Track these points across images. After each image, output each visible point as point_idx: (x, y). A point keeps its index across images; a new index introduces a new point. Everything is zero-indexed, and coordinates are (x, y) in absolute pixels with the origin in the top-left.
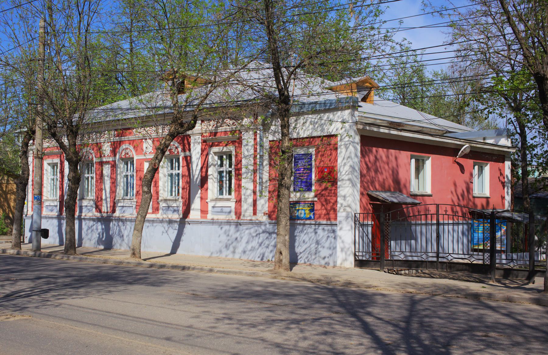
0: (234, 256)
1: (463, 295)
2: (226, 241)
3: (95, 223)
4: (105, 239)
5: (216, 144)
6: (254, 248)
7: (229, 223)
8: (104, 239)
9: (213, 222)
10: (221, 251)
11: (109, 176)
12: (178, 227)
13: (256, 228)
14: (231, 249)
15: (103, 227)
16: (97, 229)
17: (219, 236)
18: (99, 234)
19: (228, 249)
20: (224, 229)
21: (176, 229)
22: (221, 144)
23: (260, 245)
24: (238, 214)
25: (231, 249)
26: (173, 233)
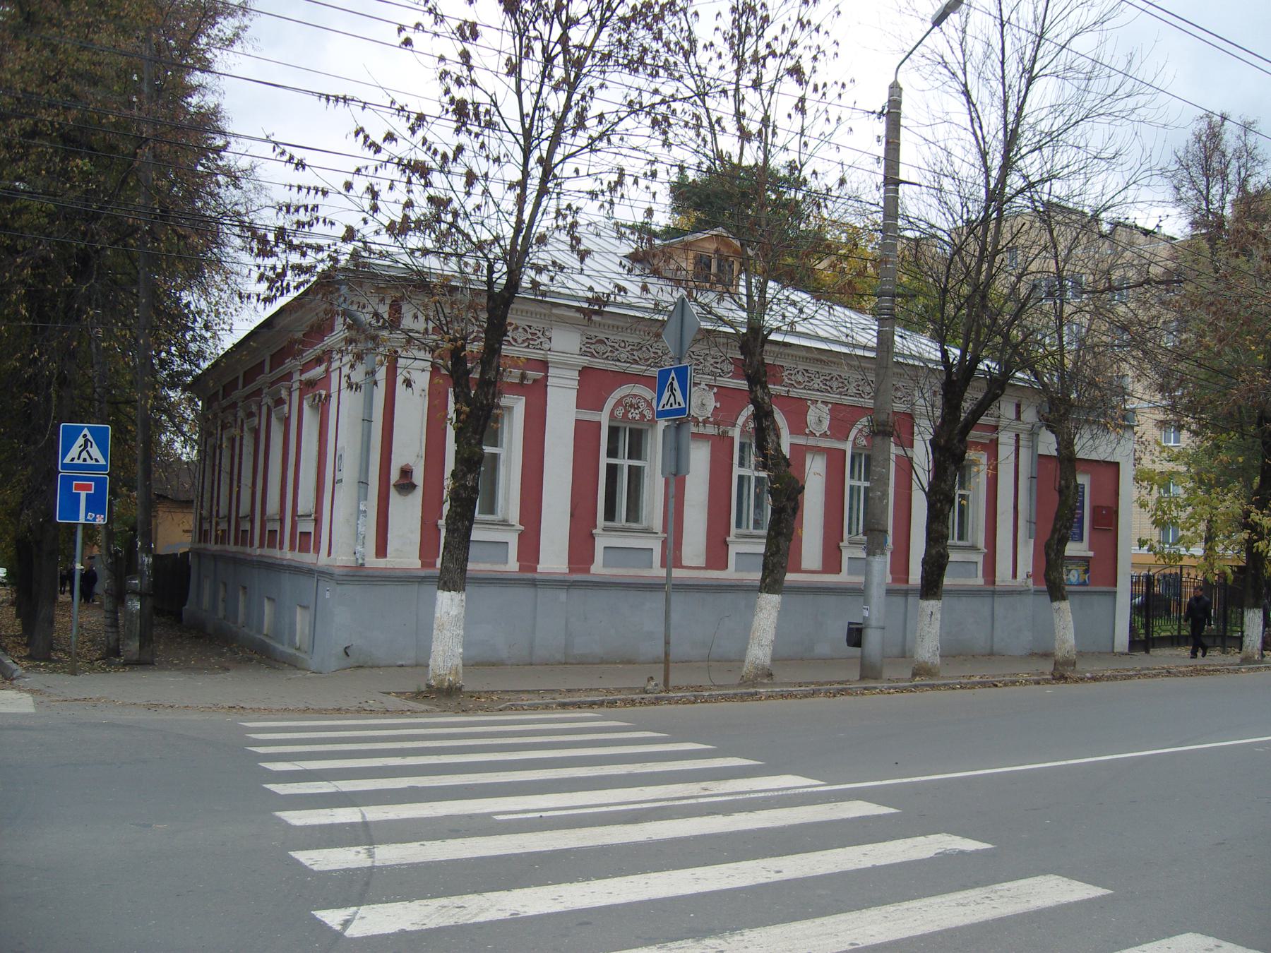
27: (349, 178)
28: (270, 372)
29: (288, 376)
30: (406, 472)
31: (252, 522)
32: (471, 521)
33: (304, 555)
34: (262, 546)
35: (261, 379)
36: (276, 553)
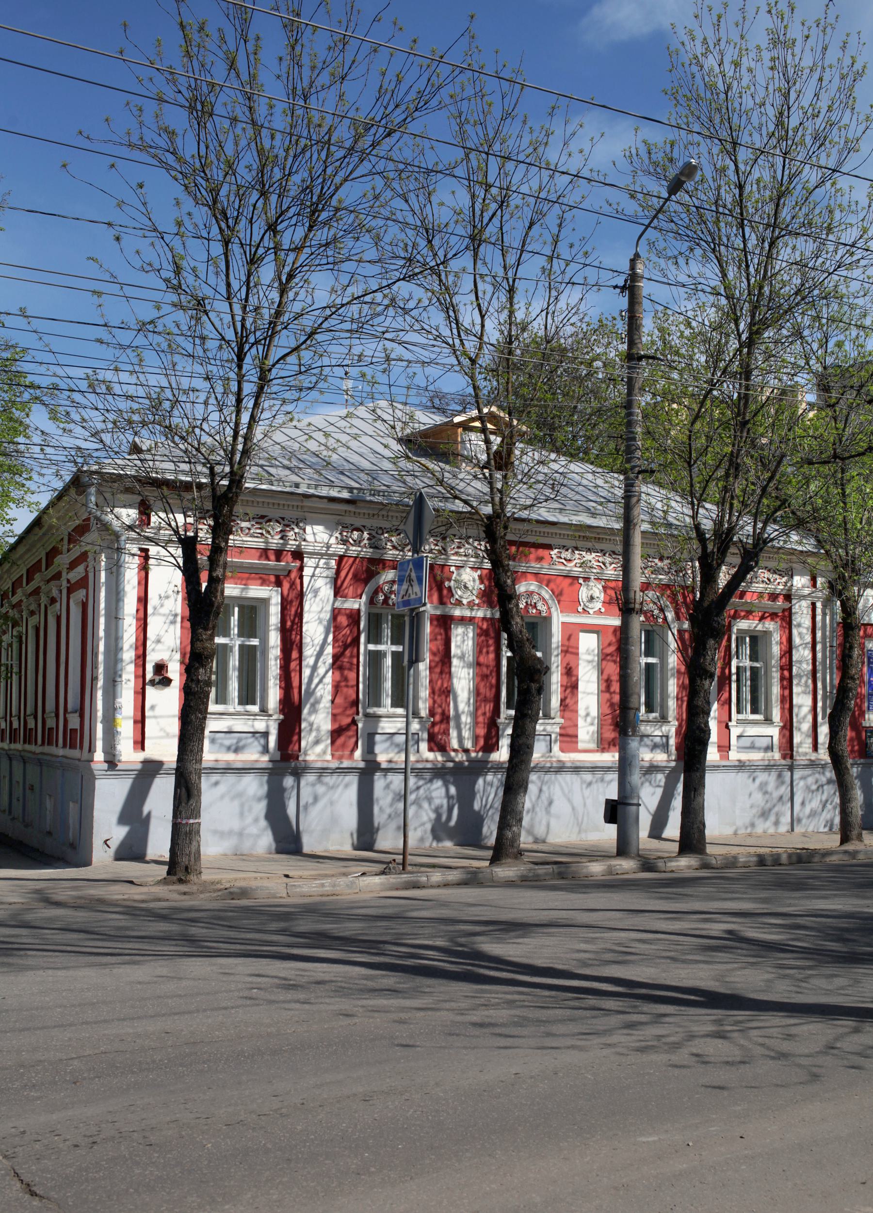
0: (777, 829)
1: (134, 441)
2: (763, 804)
3: (421, 783)
4: (457, 823)
5: (743, 614)
6: (816, 812)
7: (768, 767)
8: (453, 823)
9: (741, 766)
10: (753, 825)
11: (470, 658)
12: (664, 780)
13: (817, 776)
14: (772, 818)
15: (453, 790)
16: (430, 800)
17: (750, 795)
18: (437, 811)
19: (766, 819)
20: (758, 781)
21: (659, 786)
22: (751, 617)
23: (824, 806)
24: (788, 747)
25: (772, 818)
26: (653, 794)
27: (397, 29)
28: (46, 569)
29: (58, 576)
30: (160, 668)
31: (36, 718)
32: (205, 712)
33: (72, 751)
34: (65, 746)
35: (58, 560)
36: (53, 750)
